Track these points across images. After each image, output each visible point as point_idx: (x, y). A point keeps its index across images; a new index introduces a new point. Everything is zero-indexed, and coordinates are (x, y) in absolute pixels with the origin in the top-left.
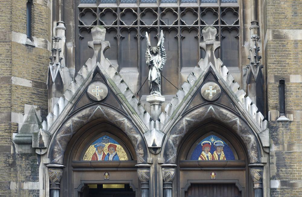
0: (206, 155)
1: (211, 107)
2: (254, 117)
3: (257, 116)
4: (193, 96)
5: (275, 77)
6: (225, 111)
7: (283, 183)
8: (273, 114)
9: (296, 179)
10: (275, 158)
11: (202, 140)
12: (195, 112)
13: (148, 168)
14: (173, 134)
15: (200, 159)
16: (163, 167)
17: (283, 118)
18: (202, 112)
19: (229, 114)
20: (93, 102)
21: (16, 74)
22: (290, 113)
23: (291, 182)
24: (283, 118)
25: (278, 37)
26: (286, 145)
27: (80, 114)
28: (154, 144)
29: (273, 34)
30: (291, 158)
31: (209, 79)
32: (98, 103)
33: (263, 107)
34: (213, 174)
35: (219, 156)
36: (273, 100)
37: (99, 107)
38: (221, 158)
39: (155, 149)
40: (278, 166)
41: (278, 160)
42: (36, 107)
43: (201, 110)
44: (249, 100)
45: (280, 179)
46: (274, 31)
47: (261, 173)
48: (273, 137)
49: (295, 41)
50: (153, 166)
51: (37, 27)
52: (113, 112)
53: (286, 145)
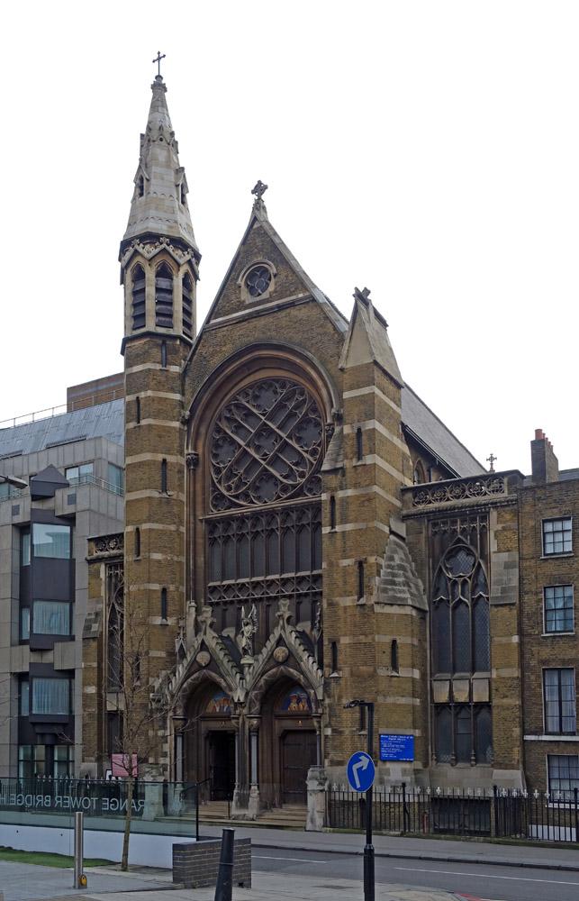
0: (293, 705)
1: (282, 667)
2: (315, 674)
4: (269, 659)
6: (291, 670)
7: (334, 731)
13: (238, 718)
17: (335, 675)
18: (274, 673)
19: (295, 673)
20: (201, 668)
22: (340, 670)
24: (335, 675)
25: (331, 604)
27: (192, 677)
28: (239, 700)
32: (204, 668)
33: (321, 666)
36: (327, 661)
38: (305, 708)
39: (240, 704)
41: (330, 710)
42: (169, 672)
43: (274, 670)
44: (311, 659)
45: (331, 727)
46: (328, 600)
47: (319, 722)
51: (170, 608)
52: (214, 674)
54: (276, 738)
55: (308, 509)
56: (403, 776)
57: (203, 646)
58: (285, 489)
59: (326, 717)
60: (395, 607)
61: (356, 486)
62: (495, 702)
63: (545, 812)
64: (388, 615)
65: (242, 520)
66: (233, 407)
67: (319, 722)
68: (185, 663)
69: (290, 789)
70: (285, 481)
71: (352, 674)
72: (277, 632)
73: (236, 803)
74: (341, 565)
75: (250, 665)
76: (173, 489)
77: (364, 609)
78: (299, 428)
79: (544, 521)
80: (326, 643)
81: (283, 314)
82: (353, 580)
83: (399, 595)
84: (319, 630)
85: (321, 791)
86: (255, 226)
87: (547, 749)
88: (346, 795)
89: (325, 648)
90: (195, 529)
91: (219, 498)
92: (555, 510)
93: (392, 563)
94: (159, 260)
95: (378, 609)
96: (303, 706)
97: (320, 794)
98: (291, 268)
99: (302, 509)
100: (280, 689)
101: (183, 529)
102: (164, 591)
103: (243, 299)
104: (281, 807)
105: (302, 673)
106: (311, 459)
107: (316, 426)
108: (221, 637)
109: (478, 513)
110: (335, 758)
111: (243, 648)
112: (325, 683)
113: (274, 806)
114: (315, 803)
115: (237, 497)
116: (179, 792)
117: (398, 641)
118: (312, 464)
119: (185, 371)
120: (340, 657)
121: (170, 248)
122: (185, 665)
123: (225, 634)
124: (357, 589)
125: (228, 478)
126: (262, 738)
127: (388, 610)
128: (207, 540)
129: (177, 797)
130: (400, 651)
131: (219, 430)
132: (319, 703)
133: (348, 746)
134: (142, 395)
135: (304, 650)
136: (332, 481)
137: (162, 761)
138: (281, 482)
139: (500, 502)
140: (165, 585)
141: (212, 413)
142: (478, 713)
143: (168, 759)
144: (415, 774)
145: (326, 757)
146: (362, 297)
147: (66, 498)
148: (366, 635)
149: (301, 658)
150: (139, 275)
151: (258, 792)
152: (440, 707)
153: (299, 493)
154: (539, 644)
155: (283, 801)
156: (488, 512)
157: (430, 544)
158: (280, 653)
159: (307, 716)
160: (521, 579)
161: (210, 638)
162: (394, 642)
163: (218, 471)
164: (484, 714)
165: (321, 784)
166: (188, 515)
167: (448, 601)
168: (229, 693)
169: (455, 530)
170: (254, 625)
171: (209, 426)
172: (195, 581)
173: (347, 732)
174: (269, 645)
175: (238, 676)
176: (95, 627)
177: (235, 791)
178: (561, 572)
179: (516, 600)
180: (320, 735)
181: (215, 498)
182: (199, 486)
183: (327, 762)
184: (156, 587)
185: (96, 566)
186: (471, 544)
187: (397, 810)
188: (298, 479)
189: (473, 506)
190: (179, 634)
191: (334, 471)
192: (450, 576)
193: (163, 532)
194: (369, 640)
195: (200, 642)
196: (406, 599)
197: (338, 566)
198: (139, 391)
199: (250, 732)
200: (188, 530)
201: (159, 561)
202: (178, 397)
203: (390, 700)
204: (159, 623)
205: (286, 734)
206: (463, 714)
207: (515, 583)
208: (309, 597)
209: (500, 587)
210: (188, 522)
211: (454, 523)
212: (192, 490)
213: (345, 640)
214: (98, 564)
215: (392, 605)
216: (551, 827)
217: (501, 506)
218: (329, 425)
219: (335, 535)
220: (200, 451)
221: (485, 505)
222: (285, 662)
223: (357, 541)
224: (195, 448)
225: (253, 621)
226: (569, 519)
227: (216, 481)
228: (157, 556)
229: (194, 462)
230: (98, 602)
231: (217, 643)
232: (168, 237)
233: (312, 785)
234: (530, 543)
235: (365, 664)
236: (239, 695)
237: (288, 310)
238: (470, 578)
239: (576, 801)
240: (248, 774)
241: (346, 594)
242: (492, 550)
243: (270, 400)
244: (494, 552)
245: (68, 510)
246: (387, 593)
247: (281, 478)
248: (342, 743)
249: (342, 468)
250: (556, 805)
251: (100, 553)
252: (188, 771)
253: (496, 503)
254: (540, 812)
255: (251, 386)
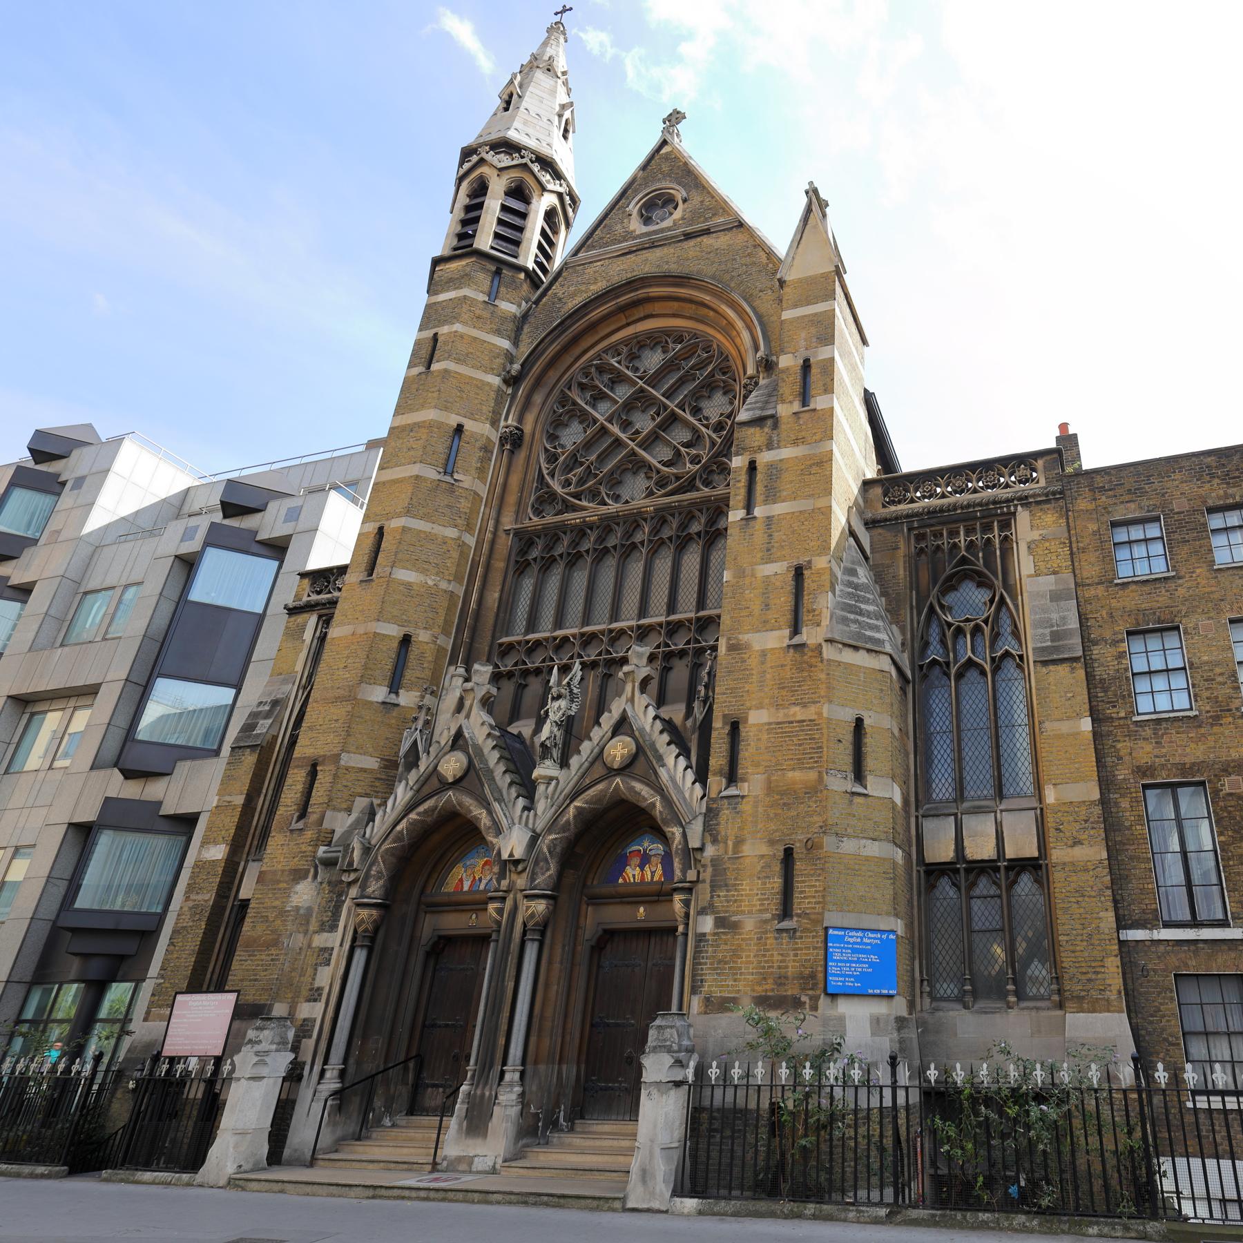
0: (632, 873)
3: (692, 790)
4: (592, 764)
5: (725, 716)
6: (638, 786)
7: (720, 922)
8: (716, 782)
9: (743, 912)
10: (709, 870)
11: (628, 845)
12: (591, 792)
13: (503, 899)
14: (550, 834)
15: (621, 881)
16: (526, 897)
17: (732, 791)
18: (601, 791)
20: (445, 785)
21: (353, 749)
22: (744, 780)
23: (733, 919)
24: (732, 791)
26: (730, 843)
27: (421, 809)
28: (511, 855)
29: (728, 643)
30: (738, 869)
31: (622, 730)
33: (702, 777)
34: (642, 909)
35: (653, 873)
36: (717, 760)
37: (618, 780)
40: (714, 887)
43: (600, 787)
45: (713, 912)
46: (729, 639)
48: (710, 829)
49: (763, 651)
50: (511, 896)
53: (730, 843)
54: (583, 950)
55: (700, 511)
56: (873, 1034)
57: (458, 740)
58: (662, 482)
59: (704, 891)
60: (862, 653)
61: (795, 442)
62: (1058, 854)
63: (1189, 1119)
64: (848, 666)
65: (581, 531)
66: (593, 370)
67: (687, 903)
68: (413, 776)
69: (596, 1082)
70: (666, 469)
71: (770, 789)
72: (616, 708)
73: (460, 1125)
74: (759, 575)
75: (551, 779)
76: (466, 472)
77: (804, 654)
78: (697, 395)
79: (1114, 524)
80: (717, 724)
81: (692, 243)
82: (784, 600)
83: (868, 633)
84: (705, 702)
85: (678, 1084)
86: (663, 151)
87: (1173, 961)
88: (741, 1093)
89: (714, 734)
90: (493, 542)
91: (546, 499)
92: (1132, 506)
93: (855, 580)
94: (515, 174)
95: (829, 652)
96: (653, 872)
97: (673, 1093)
98: (709, 193)
99: (688, 515)
100: (609, 829)
101: (471, 541)
102: (406, 640)
103: (632, 228)
104: (572, 1130)
105: (659, 789)
106: (714, 436)
107: (725, 393)
108: (504, 732)
109: (997, 515)
110: (717, 993)
111: (543, 745)
112: (709, 810)
113: (554, 1125)
114: (660, 1116)
115: (577, 496)
116: (325, 1094)
117: (867, 722)
118: (713, 443)
119: (525, 316)
120: (747, 754)
121: (536, 168)
122: (411, 783)
123: (513, 729)
124: (789, 616)
125: (568, 469)
126: (552, 948)
127: (848, 656)
128: (512, 563)
129: (317, 1107)
130: (868, 740)
131: (564, 400)
132: (690, 855)
133: (749, 963)
134: (444, 330)
135: (669, 744)
136: (755, 436)
137: (306, 1010)
138: (658, 472)
139: (1034, 496)
140: (410, 630)
141: (558, 375)
142: (1015, 882)
143: (320, 1006)
144: (899, 1029)
145: (694, 991)
146: (815, 205)
147: (283, 512)
148: (804, 705)
149: (660, 758)
150: (481, 189)
151: (518, 1089)
152: (933, 872)
153: (690, 486)
154: (1130, 735)
155: (579, 1112)
156: (1014, 514)
157: (914, 570)
158: (619, 750)
159: (660, 895)
160: (1083, 619)
161: (478, 726)
162: (859, 722)
163: (552, 458)
164: (1026, 883)
165: (679, 1063)
166: (485, 521)
167: (948, 664)
168: (495, 840)
169: (955, 546)
170: (572, 701)
171: (551, 390)
172: (474, 630)
173: (749, 924)
174: (596, 733)
175: (521, 802)
176: (263, 726)
177: (464, 1088)
178: (1156, 605)
179: (1080, 653)
180: (686, 935)
181: (540, 501)
182: (515, 480)
183: (696, 1004)
184: (394, 631)
185: (300, 619)
186: (986, 565)
187: (862, 1130)
188: (688, 465)
189: (987, 504)
190: (416, 719)
191: (758, 422)
192: (950, 619)
193: (430, 537)
194: (810, 713)
195: (453, 732)
196: (880, 642)
197: (753, 575)
198: (442, 323)
199: (524, 933)
200: (479, 543)
201: (408, 586)
202: (505, 344)
203: (849, 846)
204: (380, 699)
205: (609, 936)
206: (984, 886)
207: (1074, 624)
208: (687, 653)
209: (1048, 631)
210: (482, 531)
211: (954, 533)
212: (501, 480)
213: (757, 718)
214: (305, 616)
215: (856, 648)
216: (1211, 1163)
217: (1038, 503)
218: (751, 378)
219: (752, 523)
220: (528, 428)
221: (1008, 501)
222: (627, 768)
223: (793, 532)
224: (520, 419)
225: (571, 691)
226: (1157, 519)
227: (545, 472)
228: (404, 575)
229: (514, 441)
230: (285, 682)
231: (489, 735)
232: (533, 152)
233: (655, 1067)
234: (1093, 559)
235: (800, 765)
236: (514, 843)
237: (699, 239)
238: (986, 621)
239: (1139, 1085)
240: (502, 1041)
241: (765, 626)
242: (1025, 572)
243: (653, 360)
244: (1029, 576)
245: (279, 531)
246: (848, 626)
247: (659, 466)
248: (736, 954)
249: (772, 416)
250: (1216, 1102)
251: (314, 597)
252: (365, 1038)
253: (1026, 497)
254: (1175, 1122)
255: (626, 342)
